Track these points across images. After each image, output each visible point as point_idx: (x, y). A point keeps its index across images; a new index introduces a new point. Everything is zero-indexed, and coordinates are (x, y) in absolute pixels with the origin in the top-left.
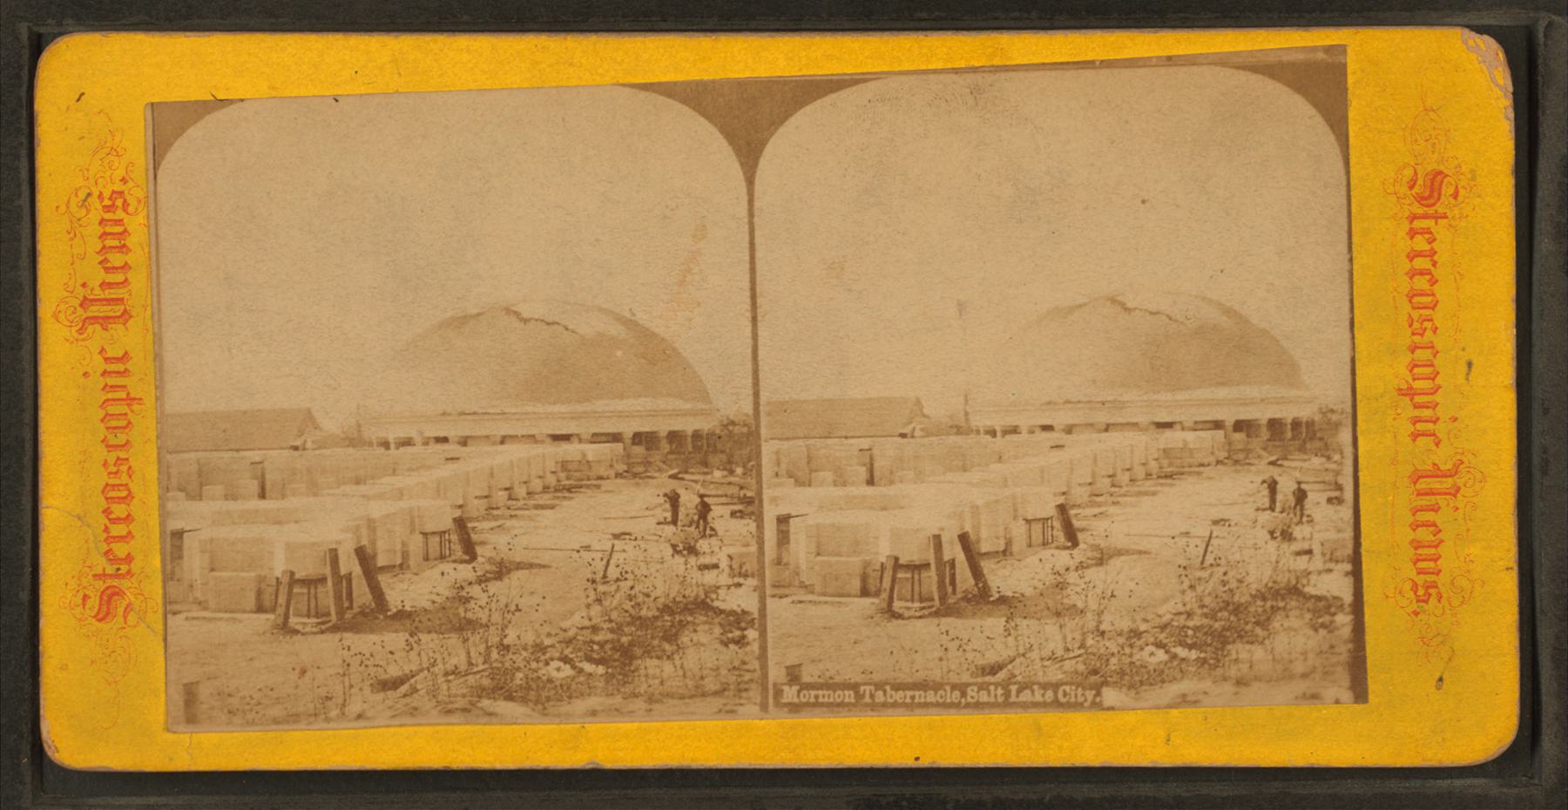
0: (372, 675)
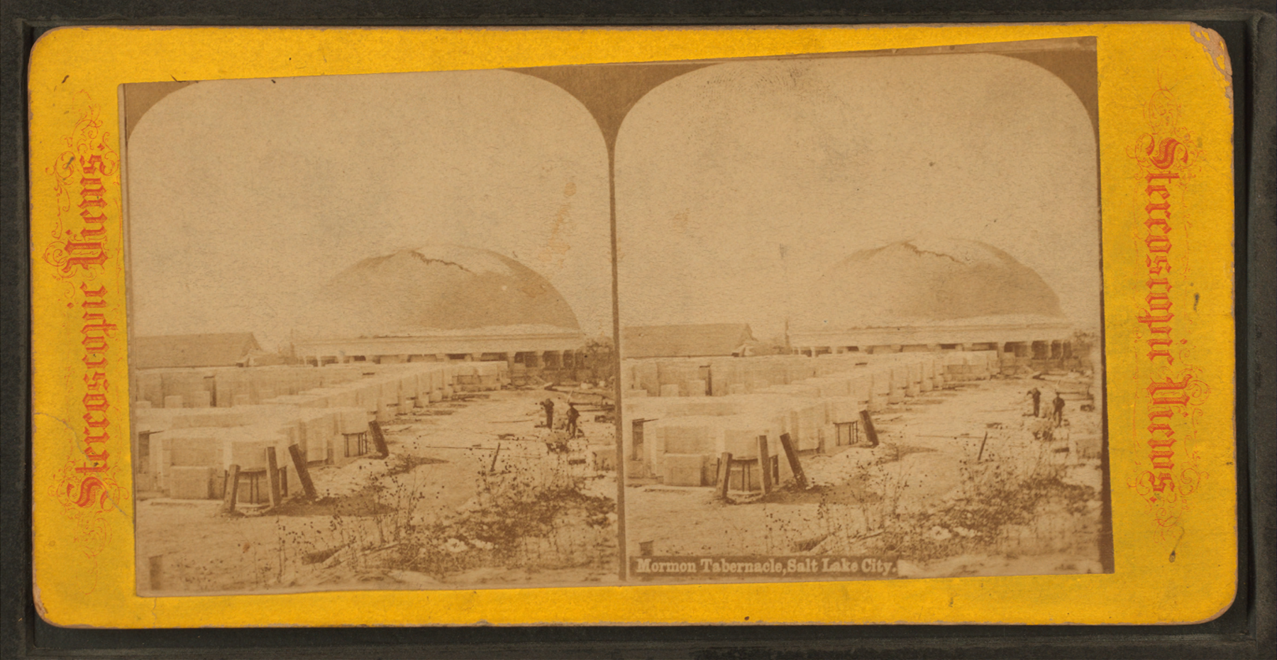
0: (303, 550)
